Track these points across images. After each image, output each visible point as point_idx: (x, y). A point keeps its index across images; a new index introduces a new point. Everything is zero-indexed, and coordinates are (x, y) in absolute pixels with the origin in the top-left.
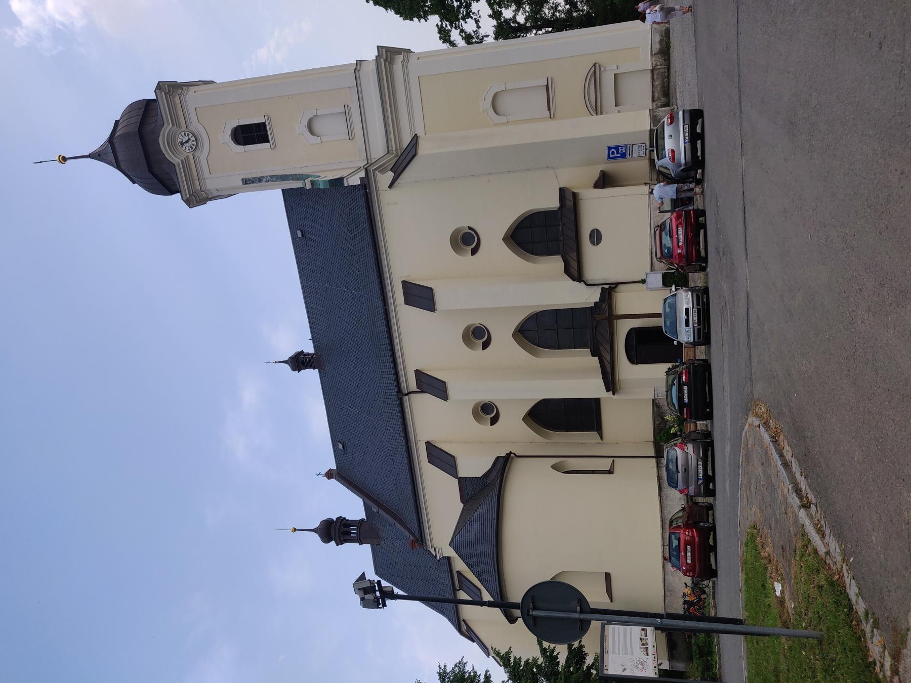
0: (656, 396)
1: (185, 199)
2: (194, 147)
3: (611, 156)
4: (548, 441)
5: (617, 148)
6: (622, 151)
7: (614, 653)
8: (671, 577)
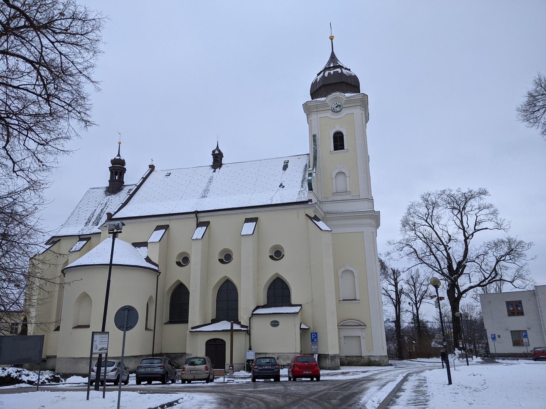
0: (187, 355)
1: (307, 103)
2: (334, 110)
3: (313, 334)
4: (165, 293)
5: (316, 337)
6: (315, 340)
7: (100, 337)
8: (85, 362)
